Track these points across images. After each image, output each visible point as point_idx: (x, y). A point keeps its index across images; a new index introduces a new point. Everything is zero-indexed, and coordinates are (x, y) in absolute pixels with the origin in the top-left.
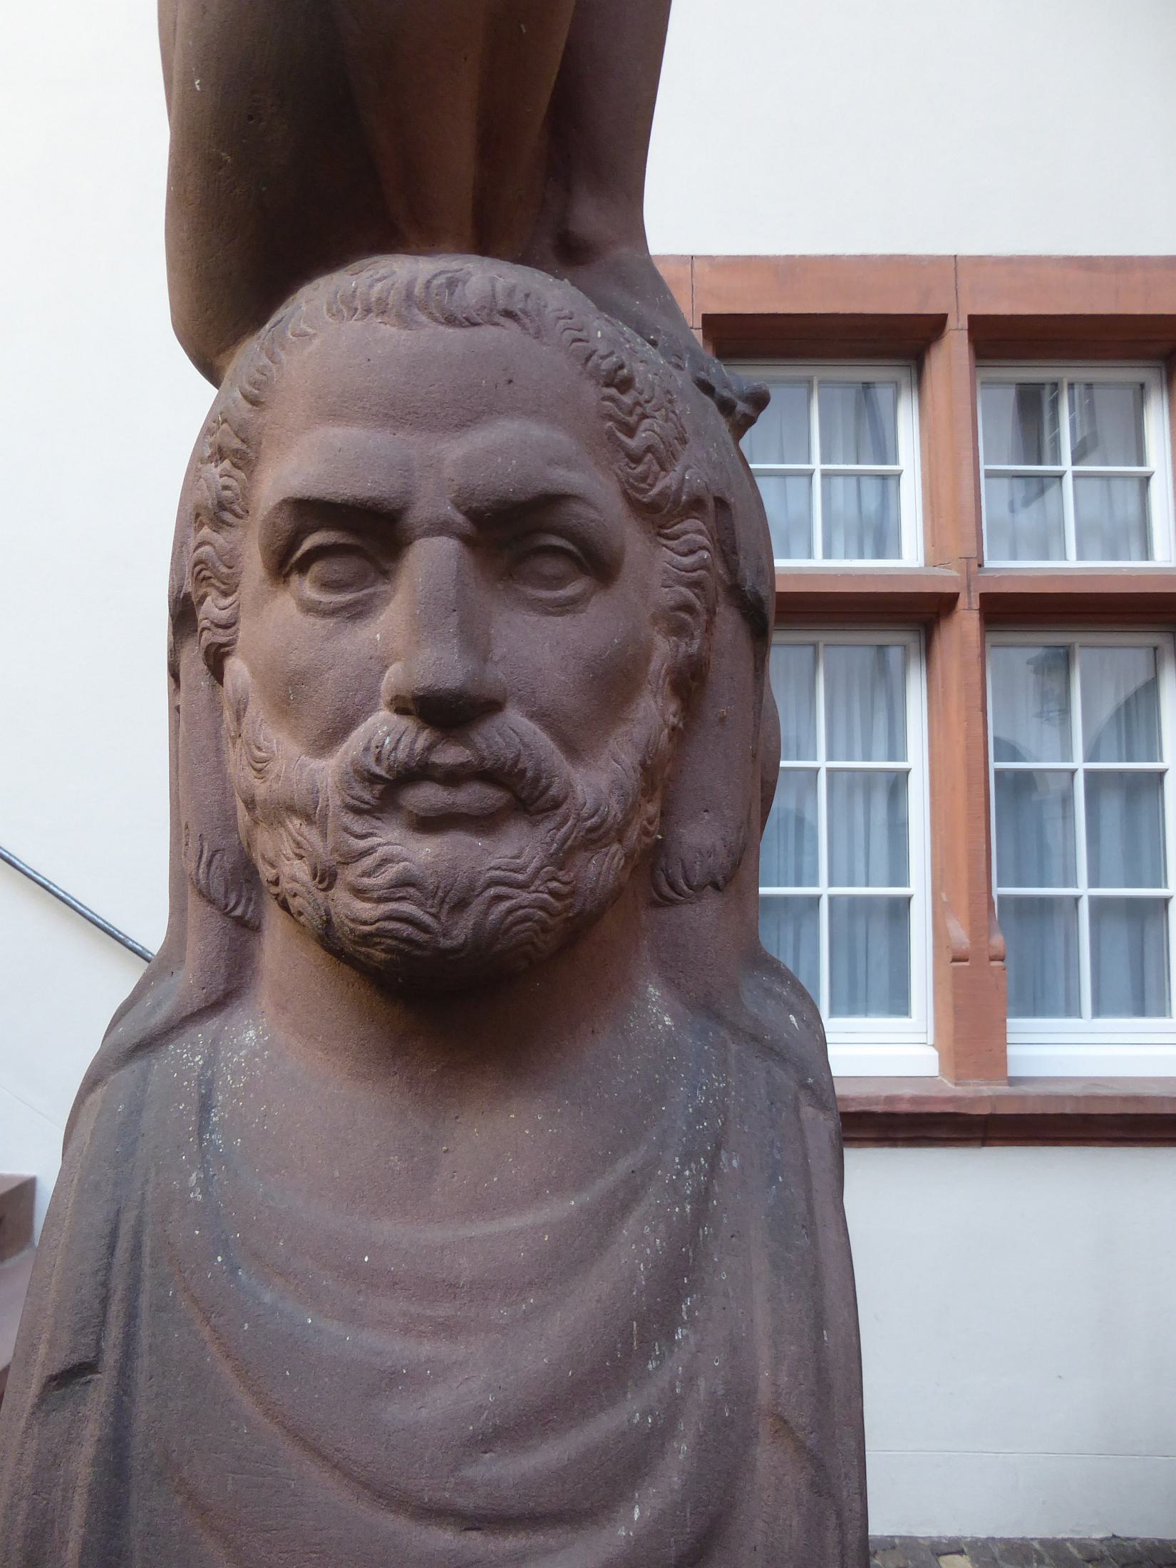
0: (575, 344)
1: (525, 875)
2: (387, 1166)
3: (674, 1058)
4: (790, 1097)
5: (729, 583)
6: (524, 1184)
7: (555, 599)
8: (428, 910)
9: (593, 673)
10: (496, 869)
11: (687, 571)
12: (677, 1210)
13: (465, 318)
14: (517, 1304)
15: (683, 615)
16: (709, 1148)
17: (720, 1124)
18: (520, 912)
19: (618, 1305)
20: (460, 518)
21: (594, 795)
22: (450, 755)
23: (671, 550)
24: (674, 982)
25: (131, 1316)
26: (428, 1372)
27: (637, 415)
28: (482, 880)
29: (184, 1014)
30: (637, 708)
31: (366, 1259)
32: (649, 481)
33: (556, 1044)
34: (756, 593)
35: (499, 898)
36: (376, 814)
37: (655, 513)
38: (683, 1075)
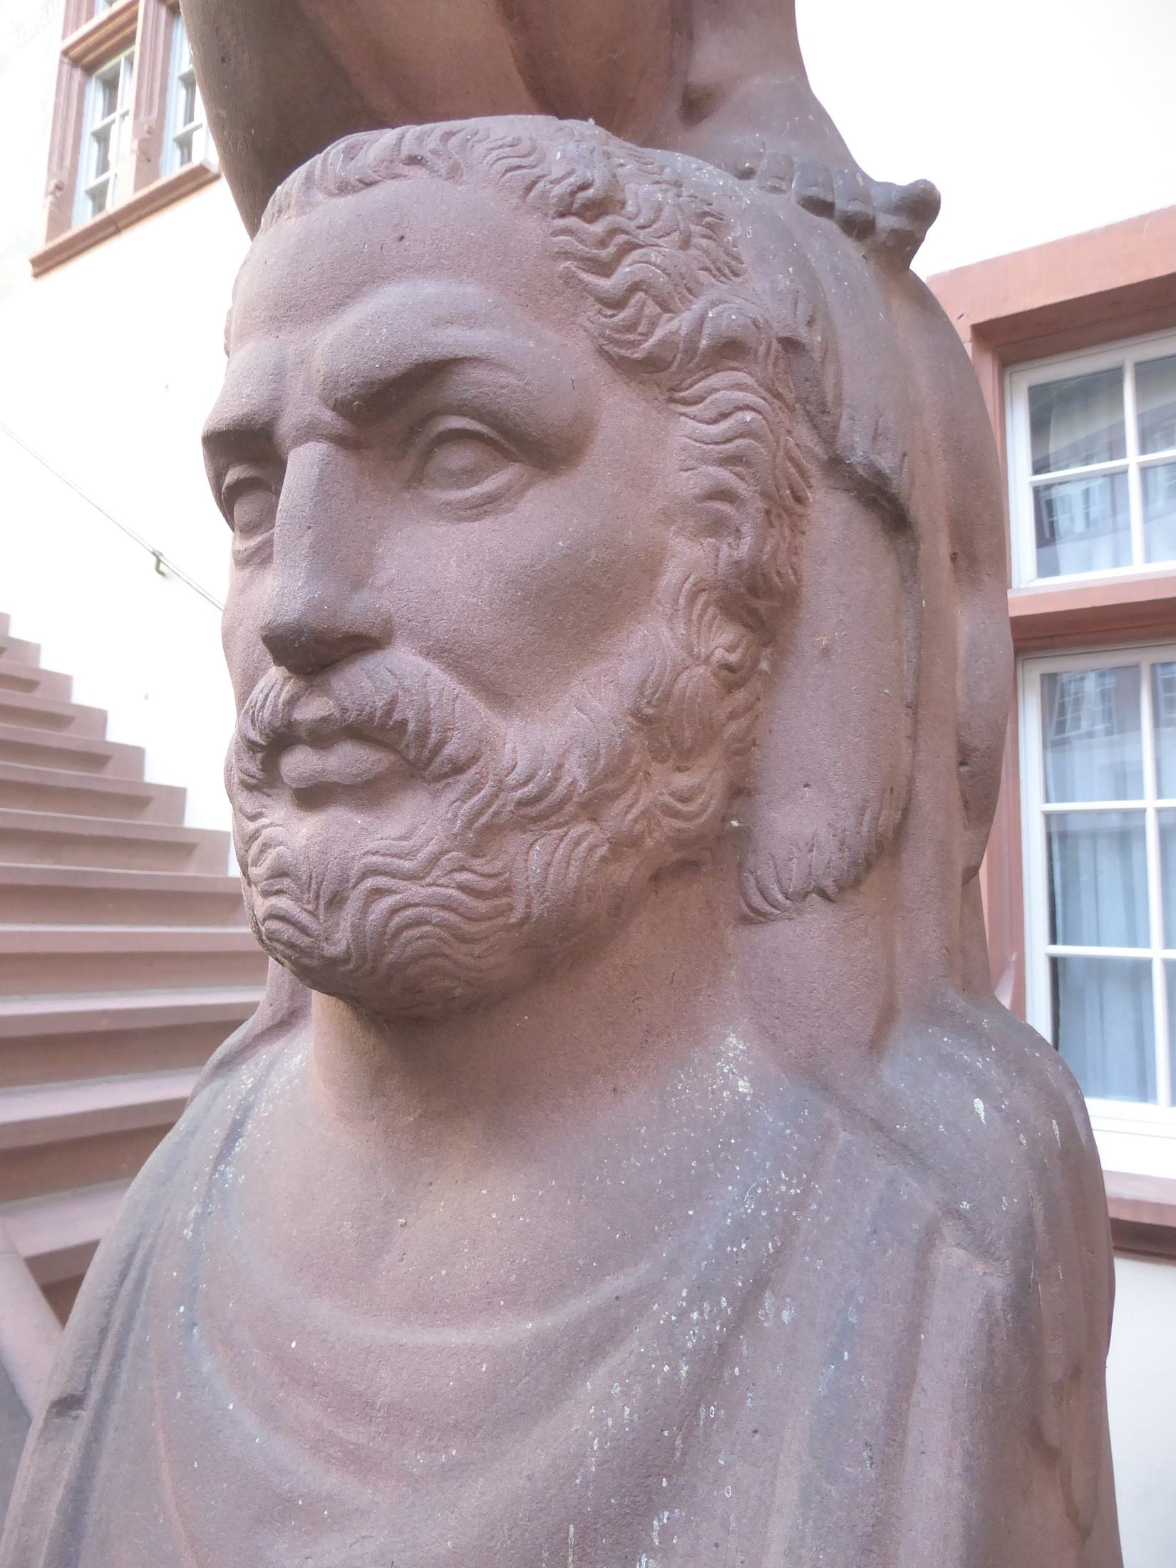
0: (509, 175)
1: (415, 862)
2: (339, 1233)
3: (733, 1141)
4: (915, 1226)
5: (825, 457)
6: (475, 1286)
7: (466, 499)
8: (305, 906)
9: (522, 590)
10: (374, 854)
11: (716, 443)
12: (666, 1368)
13: (358, 179)
14: (437, 1451)
15: (719, 505)
16: (740, 1284)
17: (771, 1250)
18: (410, 912)
19: (553, 1491)
20: (328, 415)
21: (529, 755)
22: (313, 709)
23: (693, 419)
24: (768, 1032)
25: (119, 1356)
26: (326, 1513)
27: (615, 245)
28: (356, 868)
29: (256, 1032)
30: (628, 638)
31: (294, 1345)
32: (641, 329)
33: (554, 1101)
34: (871, 466)
35: (378, 893)
36: (265, 790)
37: (658, 372)
38: (738, 1168)
